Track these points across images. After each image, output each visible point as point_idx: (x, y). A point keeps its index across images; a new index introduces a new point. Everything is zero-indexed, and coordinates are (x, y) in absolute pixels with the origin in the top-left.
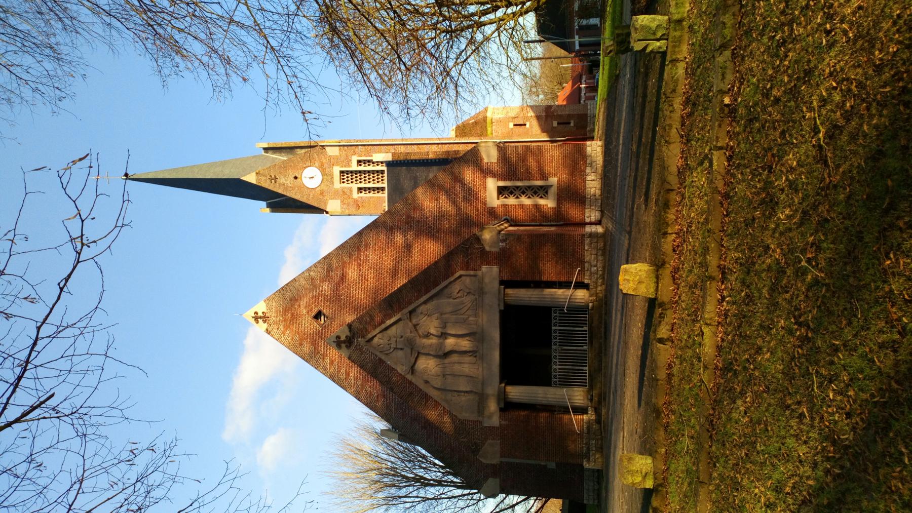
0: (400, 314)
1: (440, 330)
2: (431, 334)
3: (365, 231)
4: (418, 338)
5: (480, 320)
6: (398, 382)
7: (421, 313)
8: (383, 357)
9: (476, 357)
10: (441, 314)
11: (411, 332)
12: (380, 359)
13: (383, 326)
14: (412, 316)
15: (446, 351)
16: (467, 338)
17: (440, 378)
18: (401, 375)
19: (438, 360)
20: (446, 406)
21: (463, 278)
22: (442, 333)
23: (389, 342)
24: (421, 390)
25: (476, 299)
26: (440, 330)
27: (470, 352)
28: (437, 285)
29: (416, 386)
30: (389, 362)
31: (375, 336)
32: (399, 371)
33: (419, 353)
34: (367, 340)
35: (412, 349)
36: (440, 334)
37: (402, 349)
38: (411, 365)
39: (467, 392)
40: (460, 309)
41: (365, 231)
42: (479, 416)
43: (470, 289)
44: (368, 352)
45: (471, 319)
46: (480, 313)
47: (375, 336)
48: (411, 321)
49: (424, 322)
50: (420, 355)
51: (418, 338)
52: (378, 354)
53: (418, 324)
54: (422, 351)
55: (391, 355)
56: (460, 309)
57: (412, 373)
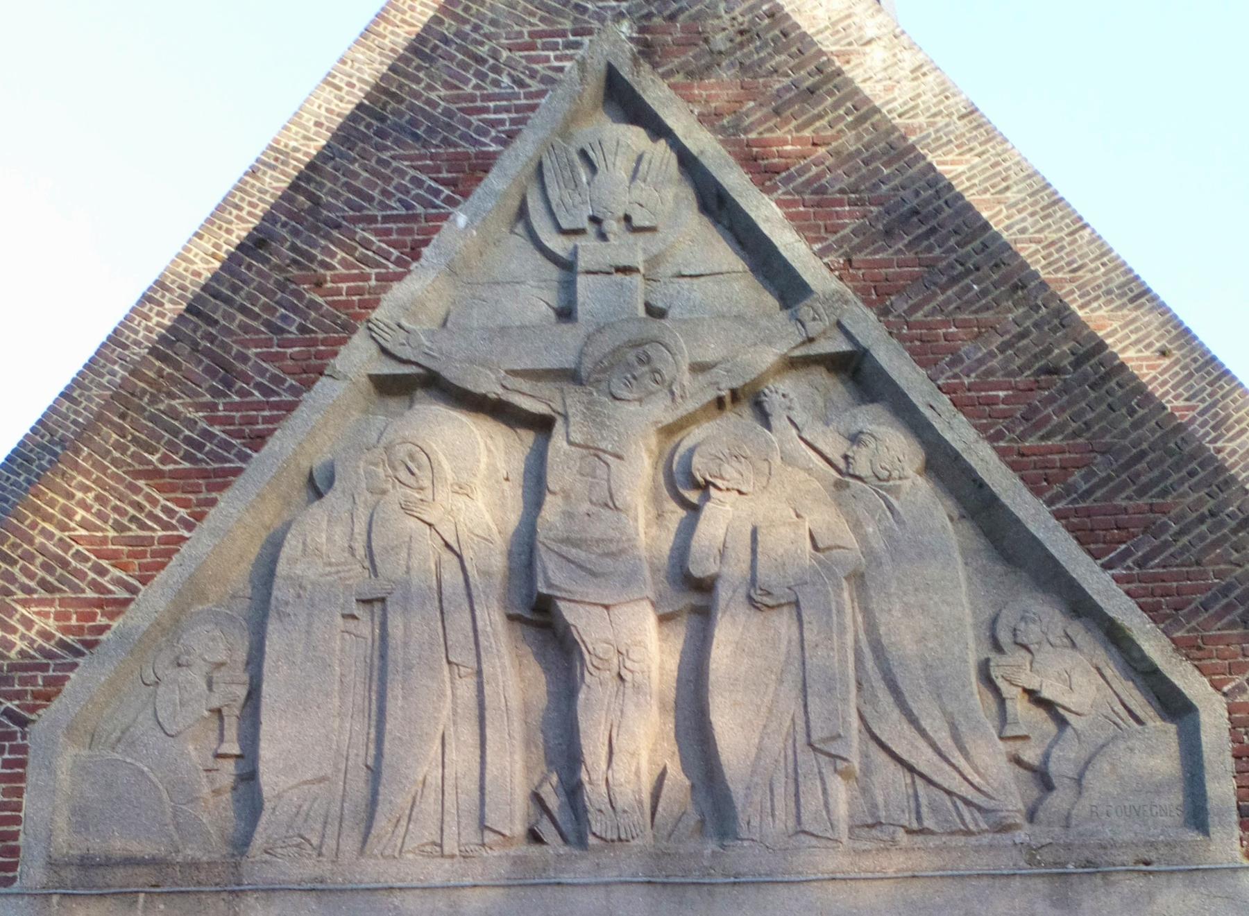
0: (835, 285)
1: (735, 570)
2: (694, 510)
3: (1155, 319)
4: (660, 411)
5: (832, 861)
6: (319, 284)
7: (855, 439)
8: (496, 181)
9: (534, 837)
10: (859, 579)
11: (699, 368)
12: (483, 165)
13: (735, 180)
14: (820, 376)
15: (570, 613)
16: (677, 777)
17: (357, 573)
18: (373, 305)
19: (498, 562)
20: (136, 618)
21: (1165, 733)
22: (704, 587)
23: (612, 226)
24: (258, 440)
25: (1004, 828)
26: (735, 570)
27: (573, 792)
28: (1084, 537)
29: (290, 407)
30: (462, 219)
31: (658, 130)
32: (399, 292)
33: (542, 425)
34: (626, 72)
35: (571, 376)
36: (697, 571)
37: (566, 313)
38: (452, 373)
39: (248, 777)
40: (913, 721)
41: (1155, 319)
42: (53, 864)
43: (1079, 781)
44: (535, 86)
45: (841, 792)
46: (895, 863)
47: (658, 130)
48: (793, 364)
49: (787, 459)
50: (529, 437)
51: (660, 411)
52: (526, 147)
53: (764, 417)
54: (558, 441)
55: (518, 241)
56: (913, 721)
57: (387, 387)
